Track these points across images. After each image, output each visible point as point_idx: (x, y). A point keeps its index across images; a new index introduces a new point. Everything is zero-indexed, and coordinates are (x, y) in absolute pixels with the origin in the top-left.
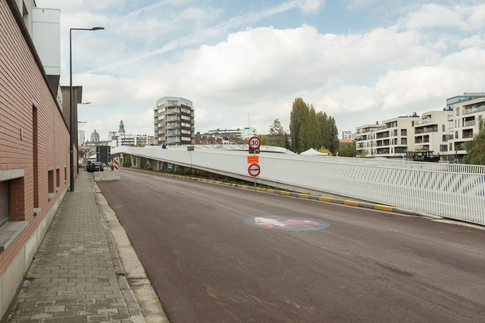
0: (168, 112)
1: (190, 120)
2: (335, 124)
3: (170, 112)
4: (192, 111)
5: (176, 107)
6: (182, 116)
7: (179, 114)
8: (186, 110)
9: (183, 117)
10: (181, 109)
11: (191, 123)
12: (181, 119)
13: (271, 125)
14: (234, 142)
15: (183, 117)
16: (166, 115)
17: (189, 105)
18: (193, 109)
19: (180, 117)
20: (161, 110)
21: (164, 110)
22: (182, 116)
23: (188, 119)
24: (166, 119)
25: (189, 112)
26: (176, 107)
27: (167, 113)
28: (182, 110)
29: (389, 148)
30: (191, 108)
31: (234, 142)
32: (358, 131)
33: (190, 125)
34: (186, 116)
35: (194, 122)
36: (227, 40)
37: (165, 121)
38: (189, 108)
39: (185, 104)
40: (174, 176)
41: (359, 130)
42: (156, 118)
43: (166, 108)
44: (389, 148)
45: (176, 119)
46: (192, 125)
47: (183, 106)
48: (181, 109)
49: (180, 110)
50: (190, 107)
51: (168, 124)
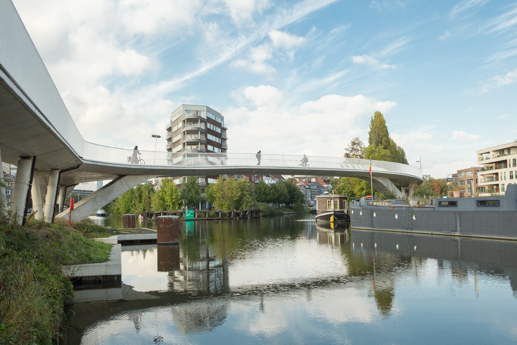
0: (187, 127)
1: (220, 142)
2: (405, 157)
3: (189, 127)
4: (224, 129)
5: (199, 120)
6: (208, 145)
7: (204, 131)
8: (215, 130)
9: (210, 137)
10: (208, 123)
11: (222, 147)
12: (207, 139)
13: (348, 147)
14: (278, 180)
15: (210, 137)
16: (184, 132)
17: (219, 120)
18: (225, 127)
19: (206, 136)
20: (176, 126)
21: (180, 125)
22: (208, 145)
23: (217, 141)
24: (184, 138)
25: (219, 130)
26: (199, 120)
27: (185, 129)
28: (209, 125)
29: (498, 184)
30: (222, 126)
31: (278, 180)
32: (480, 156)
33: (220, 150)
34: (215, 136)
35: (226, 146)
36: (215, 239)
37: (182, 142)
38: (219, 125)
39: (214, 118)
40: (82, 266)
41: (482, 154)
42: (170, 140)
43: (184, 121)
44: (498, 184)
45: (199, 138)
46: (224, 140)
47: (209, 120)
48: (208, 123)
49: (206, 125)
50: (221, 124)
51: (188, 147)
